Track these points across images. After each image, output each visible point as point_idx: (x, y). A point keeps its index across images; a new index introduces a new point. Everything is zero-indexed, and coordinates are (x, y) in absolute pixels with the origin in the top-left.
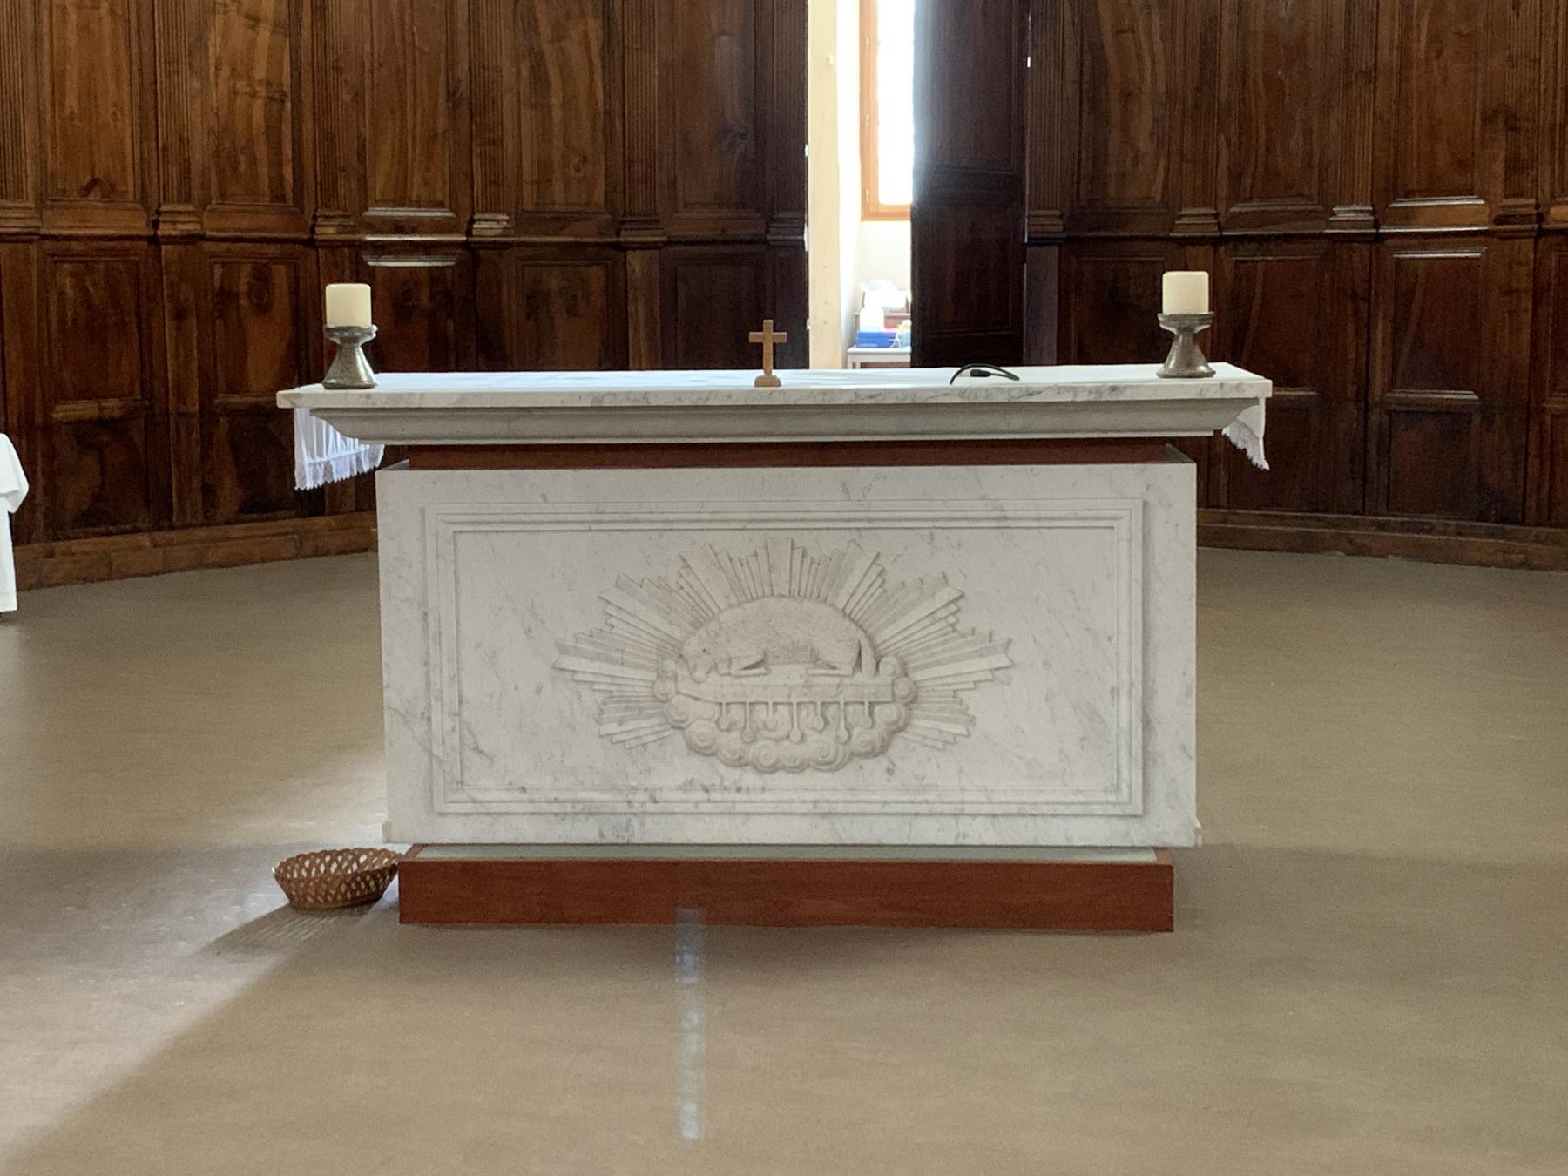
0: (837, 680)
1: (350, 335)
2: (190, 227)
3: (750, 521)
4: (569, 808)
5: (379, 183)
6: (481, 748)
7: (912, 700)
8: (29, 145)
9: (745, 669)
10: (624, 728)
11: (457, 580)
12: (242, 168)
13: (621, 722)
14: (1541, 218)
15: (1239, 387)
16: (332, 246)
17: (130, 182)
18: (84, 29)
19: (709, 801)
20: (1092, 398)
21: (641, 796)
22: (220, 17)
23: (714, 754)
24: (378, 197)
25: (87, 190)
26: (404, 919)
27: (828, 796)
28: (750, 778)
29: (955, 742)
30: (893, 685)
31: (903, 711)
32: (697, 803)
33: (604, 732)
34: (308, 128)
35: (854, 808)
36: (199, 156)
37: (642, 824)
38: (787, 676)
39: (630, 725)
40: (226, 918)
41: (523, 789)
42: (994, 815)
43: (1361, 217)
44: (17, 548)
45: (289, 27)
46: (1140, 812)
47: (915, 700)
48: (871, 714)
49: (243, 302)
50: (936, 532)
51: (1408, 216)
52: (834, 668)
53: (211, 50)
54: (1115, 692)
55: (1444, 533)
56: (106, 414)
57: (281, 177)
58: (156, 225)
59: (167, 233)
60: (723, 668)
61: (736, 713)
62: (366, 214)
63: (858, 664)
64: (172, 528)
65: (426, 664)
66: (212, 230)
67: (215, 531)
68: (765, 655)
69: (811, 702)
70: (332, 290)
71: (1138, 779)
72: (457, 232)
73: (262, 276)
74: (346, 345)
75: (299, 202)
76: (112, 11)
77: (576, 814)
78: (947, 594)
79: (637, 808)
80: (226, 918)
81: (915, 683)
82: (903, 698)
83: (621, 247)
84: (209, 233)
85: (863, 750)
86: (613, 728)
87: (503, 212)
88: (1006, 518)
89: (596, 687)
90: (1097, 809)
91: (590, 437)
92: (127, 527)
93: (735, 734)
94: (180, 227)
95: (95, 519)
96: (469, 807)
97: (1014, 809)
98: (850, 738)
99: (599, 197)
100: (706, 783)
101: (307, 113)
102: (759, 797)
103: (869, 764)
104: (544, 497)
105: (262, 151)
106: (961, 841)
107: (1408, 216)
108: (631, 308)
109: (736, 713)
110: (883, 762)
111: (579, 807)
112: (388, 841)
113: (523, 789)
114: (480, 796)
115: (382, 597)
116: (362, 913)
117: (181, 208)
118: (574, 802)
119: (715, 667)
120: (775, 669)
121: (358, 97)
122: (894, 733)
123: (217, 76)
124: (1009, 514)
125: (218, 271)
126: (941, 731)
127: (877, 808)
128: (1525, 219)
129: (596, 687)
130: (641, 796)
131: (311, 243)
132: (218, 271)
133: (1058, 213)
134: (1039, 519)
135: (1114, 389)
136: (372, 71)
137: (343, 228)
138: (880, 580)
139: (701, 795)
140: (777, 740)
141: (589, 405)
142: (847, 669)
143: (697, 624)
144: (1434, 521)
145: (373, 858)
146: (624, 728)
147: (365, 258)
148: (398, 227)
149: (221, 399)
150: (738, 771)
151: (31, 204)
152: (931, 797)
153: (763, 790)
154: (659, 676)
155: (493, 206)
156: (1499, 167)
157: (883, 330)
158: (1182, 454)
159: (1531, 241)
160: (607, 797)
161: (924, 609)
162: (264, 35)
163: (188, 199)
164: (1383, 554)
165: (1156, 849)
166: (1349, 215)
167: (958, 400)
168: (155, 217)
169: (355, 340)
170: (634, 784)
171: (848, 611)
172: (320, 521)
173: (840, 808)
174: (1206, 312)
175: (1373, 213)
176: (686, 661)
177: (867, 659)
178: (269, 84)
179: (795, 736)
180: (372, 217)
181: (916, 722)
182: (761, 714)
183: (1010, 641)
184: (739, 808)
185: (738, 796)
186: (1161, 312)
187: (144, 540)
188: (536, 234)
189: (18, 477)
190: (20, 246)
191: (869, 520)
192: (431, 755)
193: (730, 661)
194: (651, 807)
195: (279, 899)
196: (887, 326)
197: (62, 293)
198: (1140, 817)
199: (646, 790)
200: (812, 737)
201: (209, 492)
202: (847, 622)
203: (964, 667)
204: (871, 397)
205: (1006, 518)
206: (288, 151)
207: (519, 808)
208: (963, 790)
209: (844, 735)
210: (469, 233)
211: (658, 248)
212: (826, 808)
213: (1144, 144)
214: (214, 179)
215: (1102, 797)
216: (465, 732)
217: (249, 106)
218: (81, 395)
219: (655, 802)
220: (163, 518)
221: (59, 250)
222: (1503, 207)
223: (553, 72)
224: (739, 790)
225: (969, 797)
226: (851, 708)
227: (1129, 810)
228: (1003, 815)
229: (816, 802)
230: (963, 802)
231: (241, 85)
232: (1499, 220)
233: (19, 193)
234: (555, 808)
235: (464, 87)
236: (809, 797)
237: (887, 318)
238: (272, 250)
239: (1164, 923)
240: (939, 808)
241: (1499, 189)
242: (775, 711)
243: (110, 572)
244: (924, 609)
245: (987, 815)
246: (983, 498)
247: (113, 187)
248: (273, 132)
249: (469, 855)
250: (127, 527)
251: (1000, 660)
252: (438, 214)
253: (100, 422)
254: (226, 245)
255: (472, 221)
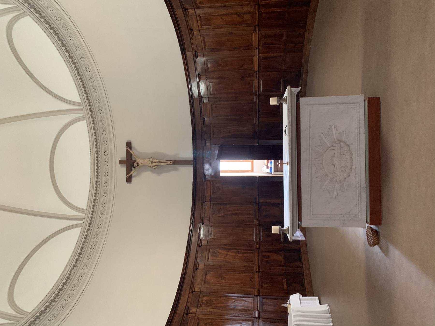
0: (337, 153)
1: (280, 230)
2: (257, 266)
3: (310, 167)
4: (360, 197)
5: (250, 238)
6: (349, 211)
7: (340, 141)
8: (245, 289)
9: (335, 167)
10: (346, 188)
11: (321, 214)
12: (248, 258)
13: (344, 188)
14: (257, 72)
15: (289, 91)
16: (259, 246)
17: (250, 275)
18: (229, 279)
19: (358, 174)
20: (290, 113)
21: (357, 185)
22: (227, 260)
23: (350, 173)
24: (252, 238)
25: (252, 281)
26: (380, 224)
27: (357, 154)
28: (354, 167)
29: (347, 134)
30: (337, 144)
31: (342, 142)
32: (358, 176)
33: (346, 191)
34: (243, 248)
35: (359, 150)
36: (246, 264)
37: (362, 185)
38: (336, 161)
39: (345, 187)
40: (381, 255)
41: (356, 205)
42: (359, 127)
43: (256, 97)
44: (307, 295)
45: (228, 250)
46: (358, 104)
47: (340, 140)
48: (342, 147)
49: (268, 259)
50: (311, 137)
51: (256, 91)
52: (335, 154)
53: (231, 261)
54: (338, 109)
55: (302, 82)
56: (286, 281)
57: (250, 252)
58: (257, 271)
59: (258, 270)
60: (335, 171)
61: (342, 169)
62: (255, 240)
63: (334, 149)
64: (303, 273)
65: (335, 220)
66: (257, 263)
67: (304, 267)
68: (333, 164)
69: (341, 157)
70: (273, 232)
71: (353, 104)
72: (257, 227)
73: (264, 256)
74: (282, 230)
75: (253, 250)
76: (226, 275)
77: (361, 196)
78: (322, 136)
79: (359, 186)
80: (381, 255)
81: (337, 140)
82: (339, 142)
83: (259, 203)
84: (258, 264)
85: (349, 149)
86: (345, 190)
87: (254, 220)
88: (309, 127)
89: (338, 192)
90: (358, 111)
91: (296, 191)
92: (303, 280)
93: (346, 169)
94: (257, 268)
95: (302, 284)
96: (360, 214)
97: (358, 124)
98: (347, 151)
99: (251, 206)
100: (355, 174)
101: (240, 248)
102: (357, 165)
103: (351, 148)
104: (306, 200)
105: (246, 255)
106: (364, 133)
107: (256, 91)
108: (268, 202)
109: (342, 169)
110: (351, 145)
111: (359, 195)
112: (366, 228)
113: (356, 205)
114: (358, 212)
115: (323, 227)
116: (379, 232)
117: (254, 267)
118: (358, 196)
119: (335, 173)
120: (335, 163)
121: (238, 240)
122: (346, 144)
123: (235, 261)
124: (309, 126)
125: (263, 263)
126: (345, 136)
127: (359, 146)
128: (257, 74)
129: (338, 192)
130: (357, 185)
131: (259, 249)
132: (263, 263)
133: (254, 140)
134: (309, 121)
135: (289, 110)
136: (234, 238)
137: (257, 244)
138: (320, 146)
139: (357, 175)
140: (347, 162)
141: (291, 191)
142: (335, 151)
143: (327, 176)
144: (300, 84)
145: (368, 232)
146: (346, 188)
147: (261, 241)
148: (256, 236)
149: (283, 264)
150: (353, 169)
151: (254, 290)
152: (356, 137)
153: (356, 165)
154: (337, 182)
155: (253, 222)
156: (249, 78)
157: (270, 169)
158: (298, 101)
159: (260, 73)
160: (358, 191)
161: (324, 139)
162: (229, 253)
163: (253, 266)
164: (305, 91)
165: (365, 101)
166: (255, 99)
167: (290, 133)
168: (256, 271)
169: (281, 229)
170: (355, 186)
171: (325, 151)
172: (302, 251)
173: (359, 152)
174: (277, 98)
175: (255, 96)
176: (334, 177)
177: (333, 148)
178: (236, 253)
179: (346, 159)
180: (255, 239)
181: (344, 140)
182: (343, 165)
183: (330, 125)
184: (359, 169)
185: (357, 169)
186: (276, 105)
187: (305, 277)
188: (257, 215)
189: (297, 295)
190: (260, 292)
191: (310, 148)
192: (350, 220)
193: (334, 170)
194: (359, 183)
195: (377, 246)
196: (269, 168)
197: (267, 286)
198: (359, 104)
199: (356, 184)
200: (346, 157)
201: (298, 267)
202: (327, 151)
203: (334, 133)
204: (290, 147)
205: (309, 127)
206: (246, 251)
207: (360, 206)
208: (355, 132)
209: (346, 152)
210: (257, 225)
211: (259, 198)
212: (359, 155)
213: (245, 128)
214: (250, 262)
215: (356, 110)
216: (347, 214)
217: (239, 256)
218: (283, 285)
219: (358, 183)
220: (302, 274)
221: (261, 287)
222: (255, 77)
223: (234, 212)
224: (356, 169)
225: (356, 131)
226: (342, 151)
227: (358, 106)
228: (359, 126)
229: (358, 156)
230: (357, 132)
231: (236, 257)
232: (257, 78)
233: (253, 291)
234: (360, 199)
235: (236, 225)
236: (357, 157)
237: (268, 168)
238: (260, 255)
239: (378, 99)
240: (358, 136)
241: (252, 78)
242: (342, 163)
243: (311, 283)
244: (324, 139)
245: (359, 129)
246: (306, 130)
247: (251, 277)
248: (243, 253)
249: (369, 214)
250: (303, 280)
251: (333, 127)
252: (254, 230)
253: (287, 282)
254: (260, 261)
255: (255, 225)
